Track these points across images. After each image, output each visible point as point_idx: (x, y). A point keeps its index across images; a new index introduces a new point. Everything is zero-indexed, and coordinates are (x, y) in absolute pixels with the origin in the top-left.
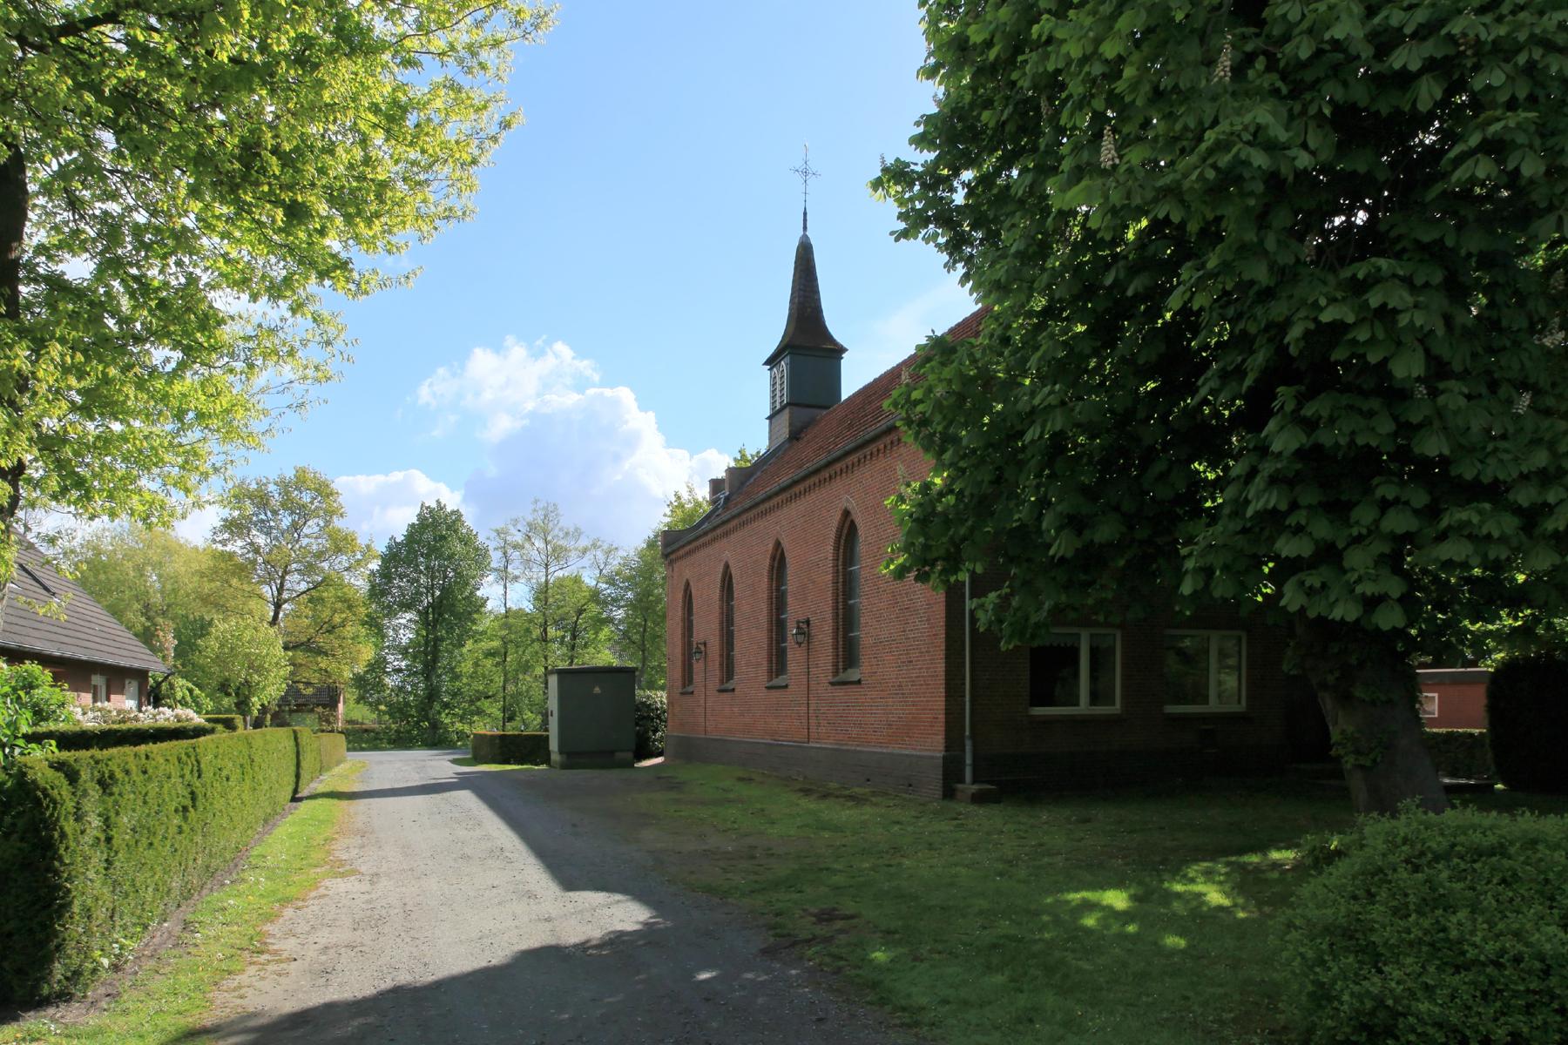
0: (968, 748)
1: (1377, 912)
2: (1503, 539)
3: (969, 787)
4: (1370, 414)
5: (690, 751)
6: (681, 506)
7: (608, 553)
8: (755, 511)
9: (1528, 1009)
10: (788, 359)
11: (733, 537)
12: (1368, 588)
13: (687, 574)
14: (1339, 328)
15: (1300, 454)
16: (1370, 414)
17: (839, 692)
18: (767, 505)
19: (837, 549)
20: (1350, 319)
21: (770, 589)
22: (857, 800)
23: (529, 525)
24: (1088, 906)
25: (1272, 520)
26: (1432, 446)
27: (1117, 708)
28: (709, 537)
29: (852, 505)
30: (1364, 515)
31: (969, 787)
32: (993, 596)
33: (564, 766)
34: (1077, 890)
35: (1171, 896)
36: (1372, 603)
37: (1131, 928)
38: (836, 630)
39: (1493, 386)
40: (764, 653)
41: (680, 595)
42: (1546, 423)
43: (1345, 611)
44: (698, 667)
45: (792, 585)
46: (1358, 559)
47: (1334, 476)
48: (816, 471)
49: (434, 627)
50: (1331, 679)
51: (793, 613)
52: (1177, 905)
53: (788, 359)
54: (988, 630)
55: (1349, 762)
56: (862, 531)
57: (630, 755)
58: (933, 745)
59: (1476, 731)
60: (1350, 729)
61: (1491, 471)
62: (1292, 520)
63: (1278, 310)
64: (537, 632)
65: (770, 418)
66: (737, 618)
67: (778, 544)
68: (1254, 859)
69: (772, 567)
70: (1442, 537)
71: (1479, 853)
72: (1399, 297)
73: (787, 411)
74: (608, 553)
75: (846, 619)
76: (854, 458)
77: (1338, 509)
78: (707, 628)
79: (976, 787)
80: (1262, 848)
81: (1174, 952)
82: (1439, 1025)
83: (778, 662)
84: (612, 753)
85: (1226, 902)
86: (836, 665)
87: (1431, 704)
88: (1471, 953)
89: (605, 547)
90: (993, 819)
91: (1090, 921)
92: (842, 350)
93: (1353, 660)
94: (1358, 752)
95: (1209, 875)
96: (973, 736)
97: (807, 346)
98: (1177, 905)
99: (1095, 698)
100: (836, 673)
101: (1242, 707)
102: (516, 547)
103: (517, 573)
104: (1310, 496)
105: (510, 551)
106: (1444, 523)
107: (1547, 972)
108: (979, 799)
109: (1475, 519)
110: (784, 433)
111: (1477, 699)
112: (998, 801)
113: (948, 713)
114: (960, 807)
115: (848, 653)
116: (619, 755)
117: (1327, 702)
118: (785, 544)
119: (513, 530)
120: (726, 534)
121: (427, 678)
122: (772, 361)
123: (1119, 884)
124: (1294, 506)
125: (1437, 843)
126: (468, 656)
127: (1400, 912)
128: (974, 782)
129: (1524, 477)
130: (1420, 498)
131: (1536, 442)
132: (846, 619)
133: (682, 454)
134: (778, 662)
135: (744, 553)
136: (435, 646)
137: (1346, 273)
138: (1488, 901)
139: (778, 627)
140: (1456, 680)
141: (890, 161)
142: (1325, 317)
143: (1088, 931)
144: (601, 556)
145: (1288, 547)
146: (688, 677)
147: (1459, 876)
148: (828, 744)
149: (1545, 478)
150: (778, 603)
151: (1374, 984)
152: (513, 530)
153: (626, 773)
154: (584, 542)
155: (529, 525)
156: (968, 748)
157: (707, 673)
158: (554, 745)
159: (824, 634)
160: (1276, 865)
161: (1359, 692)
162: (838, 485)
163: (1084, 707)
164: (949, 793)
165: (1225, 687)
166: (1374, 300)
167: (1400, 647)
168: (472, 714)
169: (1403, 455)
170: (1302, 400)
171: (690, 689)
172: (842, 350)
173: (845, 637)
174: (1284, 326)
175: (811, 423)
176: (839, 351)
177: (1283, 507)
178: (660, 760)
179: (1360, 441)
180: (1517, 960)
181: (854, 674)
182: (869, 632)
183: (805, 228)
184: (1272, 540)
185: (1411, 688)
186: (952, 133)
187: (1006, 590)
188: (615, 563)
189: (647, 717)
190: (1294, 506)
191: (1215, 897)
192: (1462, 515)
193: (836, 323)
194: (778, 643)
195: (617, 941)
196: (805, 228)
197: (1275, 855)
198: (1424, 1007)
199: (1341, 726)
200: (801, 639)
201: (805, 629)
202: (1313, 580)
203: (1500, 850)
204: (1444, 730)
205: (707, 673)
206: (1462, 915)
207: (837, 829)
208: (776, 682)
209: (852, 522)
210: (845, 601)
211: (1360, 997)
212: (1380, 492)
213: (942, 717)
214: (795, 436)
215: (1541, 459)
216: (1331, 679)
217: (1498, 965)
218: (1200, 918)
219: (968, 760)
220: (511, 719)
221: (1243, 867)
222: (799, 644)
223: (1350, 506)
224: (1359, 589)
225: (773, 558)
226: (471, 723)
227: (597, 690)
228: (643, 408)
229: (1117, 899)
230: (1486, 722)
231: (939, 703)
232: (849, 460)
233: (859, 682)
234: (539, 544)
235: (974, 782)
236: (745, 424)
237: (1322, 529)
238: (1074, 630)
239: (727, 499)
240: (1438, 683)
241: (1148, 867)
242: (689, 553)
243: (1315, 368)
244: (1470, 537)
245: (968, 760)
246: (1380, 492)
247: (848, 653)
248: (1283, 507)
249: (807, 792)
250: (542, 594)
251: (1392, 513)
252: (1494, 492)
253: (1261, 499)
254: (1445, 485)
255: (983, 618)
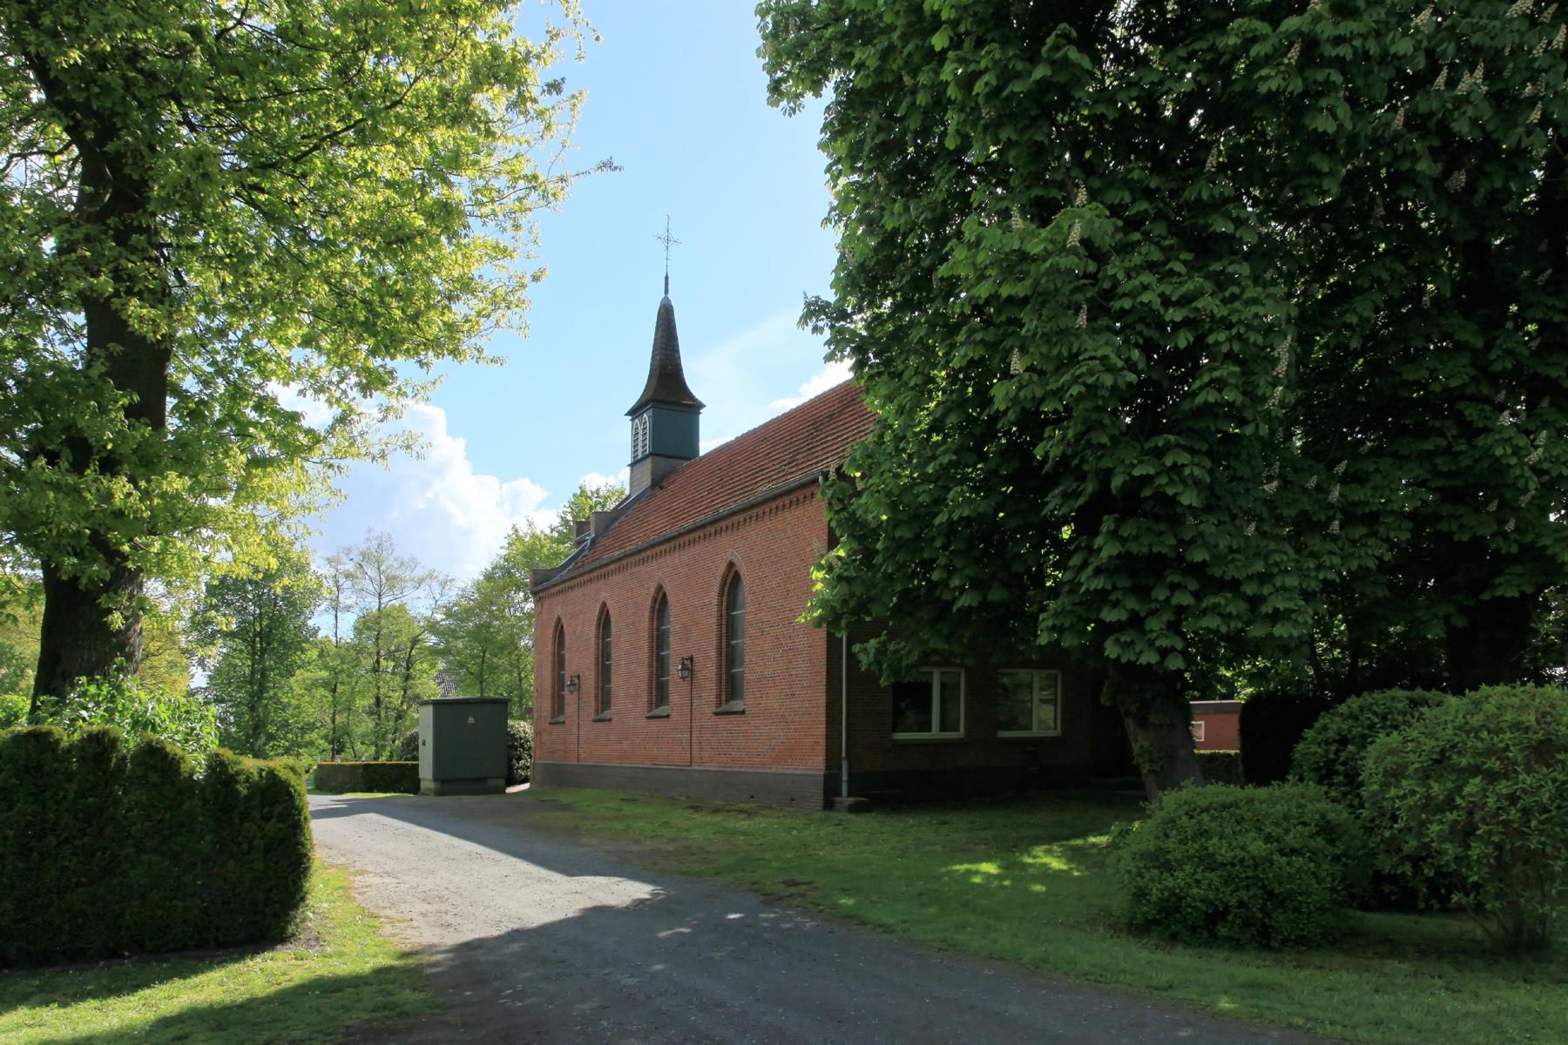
0: (845, 764)
1: (1171, 844)
2: (1239, 617)
3: (845, 799)
4: (1161, 533)
5: (559, 776)
6: (519, 538)
7: (443, 584)
8: (636, 558)
9: (1248, 887)
10: (650, 412)
11: (611, 579)
12: (1164, 642)
13: (559, 611)
14: (1147, 479)
15: (1119, 555)
16: (1161, 533)
17: (724, 722)
18: (649, 553)
19: (721, 595)
20: (1152, 472)
21: (651, 629)
22: (750, 814)
23: (363, 555)
24: (969, 873)
25: (1101, 597)
26: (1199, 555)
27: (961, 733)
28: (586, 577)
29: (738, 558)
30: (1161, 594)
31: (845, 799)
32: (873, 642)
33: (438, 793)
34: (961, 863)
35: (1024, 866)
36: (1164, 653)
37: (1007, 883)
38: (719, 667)
39: (1234, 517)
40: (645, 687)
41: (551, 631)
42: (1263, 543)
43: (1149, 658)
44: (570, 698)
45: (674, 624)
46: (1154, 624)
47: (1140, 572)
48: (703, 526)
49: (262, 656)
50: (1133, 708)
51: (676, 650)
52: (1031, 870)
53: (650, 412)
54: (868, 670)
55: (1145, 768)
56: (746, 580)
57: (502, 782)
58: (815, 764)
59: (1232, 752)
60: (1146, 745)
61: (1231, 572)
62: (1113, 597)
63: (1106, 463)
64: (368, 662)
65: (632, 465)
66: (614, 653)
67: (660, 588)
68: (1079, 842)
69: (653, 609)
70: (1204, 613)
71: (1225, 807)
72: (1184, 458)
73: (649, 460)
74: (443, 584)
75: (729, 657)
76: (741, 517)
77: (1142, 592)
78: (580, 660)
79: (851, 800)
80: (1084, 835)
81: (1038, 894)
82: (1202, 901)
83: (659, 693)
84: (484, 780)
85: (1064, 867)
86: (719, 696)
87: (1200, 730)
88: (1219, 859)
89: (441, 578)
90: (867, 823)
91: (977, 880)
92: (701, 406)
93: (1149, 696)
94: (1151, 761)
95: (1049, 852)
96: (848, 757)
97: (668, 399)
98: (1031, 870)
99: (943, 728)
100: (719, 704)
101: (1057, 732)
102: (348, 576)
103: (349, 602)
104: (1124, 582)
105: (342, 580)
106: (1204, 605)
107: (1256, 866)
108: (855, 809)
109: (1223, 602)
110: (646, 481)
111: (1232, 724)
112: (869, 810)
113: (828, 737)
114: (840, 816)
115: (730, 686)
116: (491, 782)
117: (1130, 725)
118: (668, 589)
119: (344, 559)
120: (605, 576)
121: (253, 709)
122: (634, 412)
123: (989, 859)
124: (1115, 588)
125: (1203, 803)
126: (301, 694)
127: (1183, 842)
128: (850, 795)
129: (1250, 578)
130: (1194, 585)
131: (1257, 555)
132: (729, 657)
133: (492, 481)
134: (659, 693)
135: (625, 596)
136: (263, 675)
137: (1150, 444)
138: (1228, 831)
139: (659, 665)
140: (1218, 710)
141: (811, 298)
142: (1137, 472)
143: (979, 885)
144: (437, 589)
145: (1110, 615)
146: (558, 705)
147: (1214, 819)
148: (713, 767)
149: (1264, 578)
150: (659, 640)
151: (1170, 883)
152: (344, 559)
153: (495, 798)
154: (419, 573)
155: (363, 555)
156: (845, 764)
157: (581, 705)
158: (426, 771)
159: (708, 669)
160: (1094, 845)
161: (1152, 719)
162: (723, 539)
163: (935, 733)
164: (829, 805)
165: (1044, 718)
166: (1168, 462)
167: (1179, 686)
168: (300, 746)
169: (1180, 558)
170: (1120, 522)
171: (561, 719)
172: (701, 406)
173: (728, 673)
174: (1109, 473)
175: (673, 471)
176: (696, 407)
177: (1109, 587)
178: (526, 786)
179: (1155, 550)
180: (1242, 861)
181: (737, 705)
182: (751, 669)
183: (667, 291)
184: (1099, 610)
185: (1187, 715)
186: (862, 278)
187: (883, 638)
188: (452, 595)
189: (513, 746)
190: (1115, 588)
191: (1056, 864)
192: (1217, 600)
193: (697, 376)
194: (658, 677)
195: (641, 902)
196: (667, 291)
197: (1092, 840)
198: (1196, 891)
199: (1140, 742)
200: (686, 673)
201: (689, 665)
202: (1125, 638)
203: (1236, 805)
204: (1208, 752)
205: (581, 705)
206: (1215, 840)
207: (745, 834)
208: (656, 712)
209: (737, 573)
210: (728, 642)
211: (1162, 891)
212: (1169, 579)
213: (823, 742)
214: (658, 483)
215: (1260, 567)
216: (1133, 708)
217: (1234, 865)
218: (1046, 875)
219: (845, 778)
220: (339, 752)
221: (1073, 849)
222: (683, 678)
223: (1149, 589)
224: (1158, 643)
225: (655, 600)
226: (298, 755)
227: (471, 720)
228: (452, 432)
229: (990, 868)
230: (1238, 743)
231: (821, 730)
232: (735, 519)
233: (743, 712)
234: (372, 572)
235: (850, 795)
236: (611, 472)
237: (1132, 603)
238: (956, 670)
239: (593, 541)
240: (1205, 712)
241: (1007, 848)
242: (558, 593)
243: (1130, 503)
244: (1219, 614)
245: (845, 778)
246: (1169, 579)
247: (730, 686)
248: (1109, 587)
249: (696, 809)
250: (367, 625)
251: (1177, 593)
252: (1234, 586)
253: (1092, 583)
254: (1208, 582)
255: (865, 660)
